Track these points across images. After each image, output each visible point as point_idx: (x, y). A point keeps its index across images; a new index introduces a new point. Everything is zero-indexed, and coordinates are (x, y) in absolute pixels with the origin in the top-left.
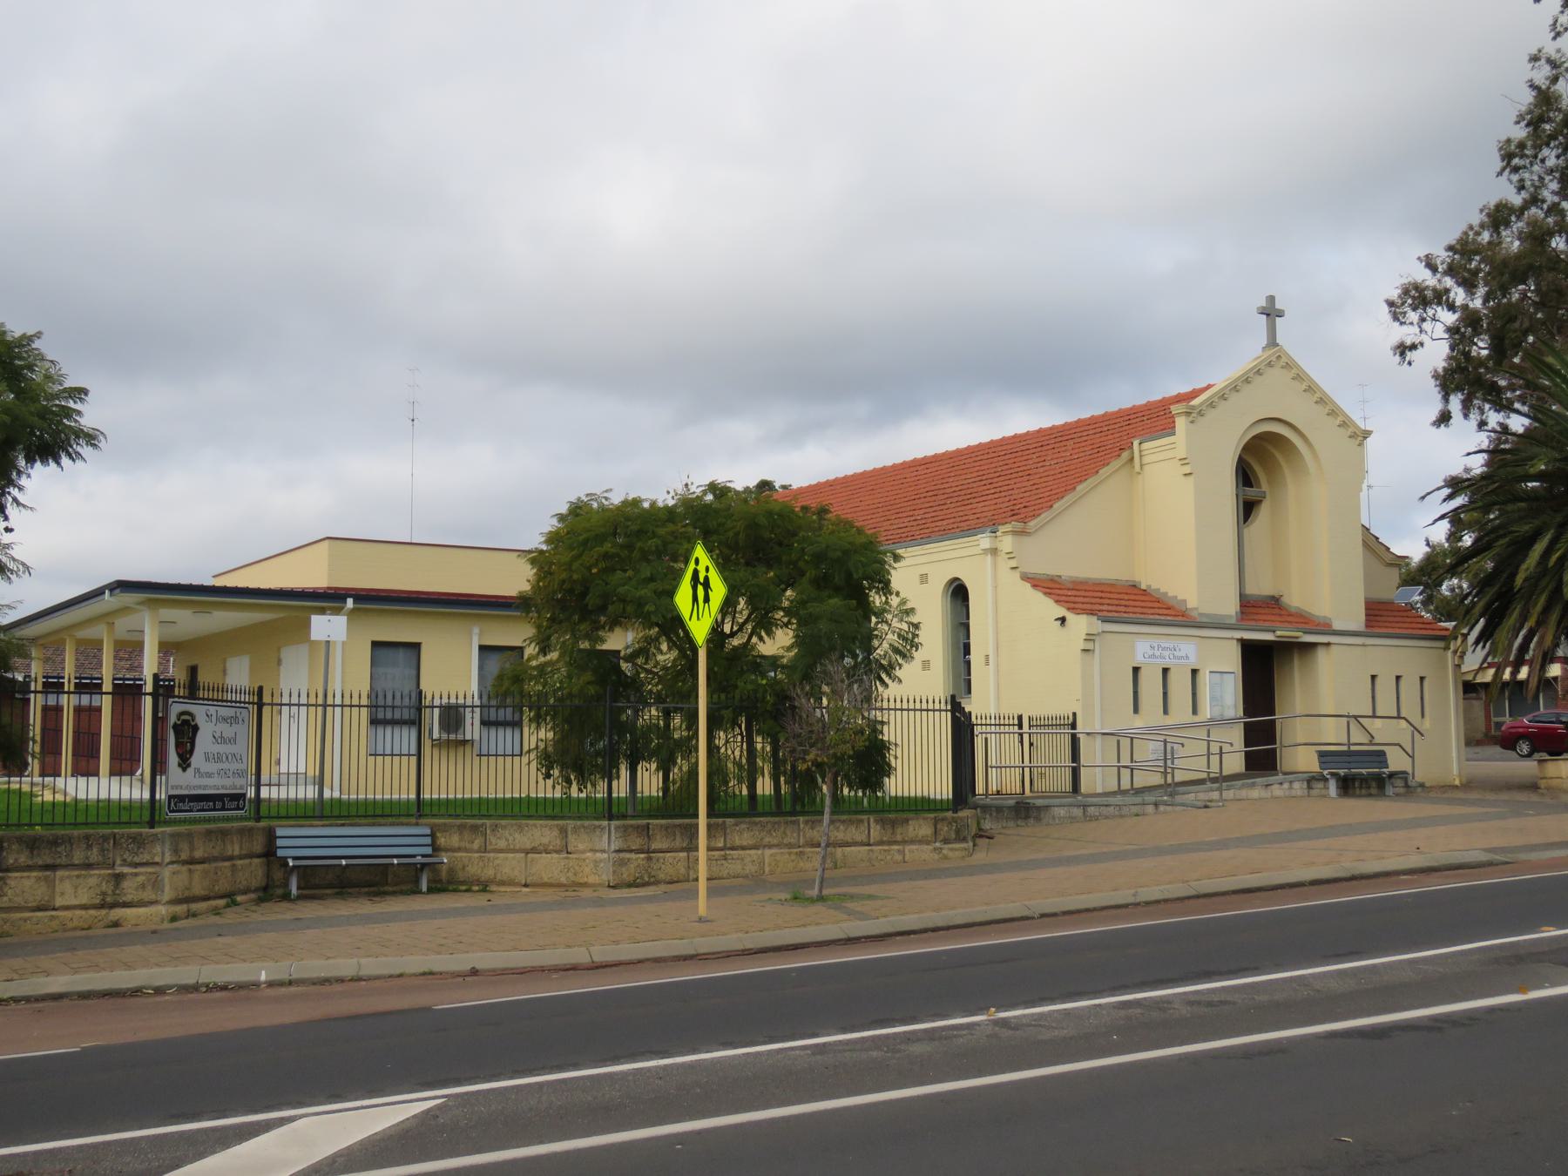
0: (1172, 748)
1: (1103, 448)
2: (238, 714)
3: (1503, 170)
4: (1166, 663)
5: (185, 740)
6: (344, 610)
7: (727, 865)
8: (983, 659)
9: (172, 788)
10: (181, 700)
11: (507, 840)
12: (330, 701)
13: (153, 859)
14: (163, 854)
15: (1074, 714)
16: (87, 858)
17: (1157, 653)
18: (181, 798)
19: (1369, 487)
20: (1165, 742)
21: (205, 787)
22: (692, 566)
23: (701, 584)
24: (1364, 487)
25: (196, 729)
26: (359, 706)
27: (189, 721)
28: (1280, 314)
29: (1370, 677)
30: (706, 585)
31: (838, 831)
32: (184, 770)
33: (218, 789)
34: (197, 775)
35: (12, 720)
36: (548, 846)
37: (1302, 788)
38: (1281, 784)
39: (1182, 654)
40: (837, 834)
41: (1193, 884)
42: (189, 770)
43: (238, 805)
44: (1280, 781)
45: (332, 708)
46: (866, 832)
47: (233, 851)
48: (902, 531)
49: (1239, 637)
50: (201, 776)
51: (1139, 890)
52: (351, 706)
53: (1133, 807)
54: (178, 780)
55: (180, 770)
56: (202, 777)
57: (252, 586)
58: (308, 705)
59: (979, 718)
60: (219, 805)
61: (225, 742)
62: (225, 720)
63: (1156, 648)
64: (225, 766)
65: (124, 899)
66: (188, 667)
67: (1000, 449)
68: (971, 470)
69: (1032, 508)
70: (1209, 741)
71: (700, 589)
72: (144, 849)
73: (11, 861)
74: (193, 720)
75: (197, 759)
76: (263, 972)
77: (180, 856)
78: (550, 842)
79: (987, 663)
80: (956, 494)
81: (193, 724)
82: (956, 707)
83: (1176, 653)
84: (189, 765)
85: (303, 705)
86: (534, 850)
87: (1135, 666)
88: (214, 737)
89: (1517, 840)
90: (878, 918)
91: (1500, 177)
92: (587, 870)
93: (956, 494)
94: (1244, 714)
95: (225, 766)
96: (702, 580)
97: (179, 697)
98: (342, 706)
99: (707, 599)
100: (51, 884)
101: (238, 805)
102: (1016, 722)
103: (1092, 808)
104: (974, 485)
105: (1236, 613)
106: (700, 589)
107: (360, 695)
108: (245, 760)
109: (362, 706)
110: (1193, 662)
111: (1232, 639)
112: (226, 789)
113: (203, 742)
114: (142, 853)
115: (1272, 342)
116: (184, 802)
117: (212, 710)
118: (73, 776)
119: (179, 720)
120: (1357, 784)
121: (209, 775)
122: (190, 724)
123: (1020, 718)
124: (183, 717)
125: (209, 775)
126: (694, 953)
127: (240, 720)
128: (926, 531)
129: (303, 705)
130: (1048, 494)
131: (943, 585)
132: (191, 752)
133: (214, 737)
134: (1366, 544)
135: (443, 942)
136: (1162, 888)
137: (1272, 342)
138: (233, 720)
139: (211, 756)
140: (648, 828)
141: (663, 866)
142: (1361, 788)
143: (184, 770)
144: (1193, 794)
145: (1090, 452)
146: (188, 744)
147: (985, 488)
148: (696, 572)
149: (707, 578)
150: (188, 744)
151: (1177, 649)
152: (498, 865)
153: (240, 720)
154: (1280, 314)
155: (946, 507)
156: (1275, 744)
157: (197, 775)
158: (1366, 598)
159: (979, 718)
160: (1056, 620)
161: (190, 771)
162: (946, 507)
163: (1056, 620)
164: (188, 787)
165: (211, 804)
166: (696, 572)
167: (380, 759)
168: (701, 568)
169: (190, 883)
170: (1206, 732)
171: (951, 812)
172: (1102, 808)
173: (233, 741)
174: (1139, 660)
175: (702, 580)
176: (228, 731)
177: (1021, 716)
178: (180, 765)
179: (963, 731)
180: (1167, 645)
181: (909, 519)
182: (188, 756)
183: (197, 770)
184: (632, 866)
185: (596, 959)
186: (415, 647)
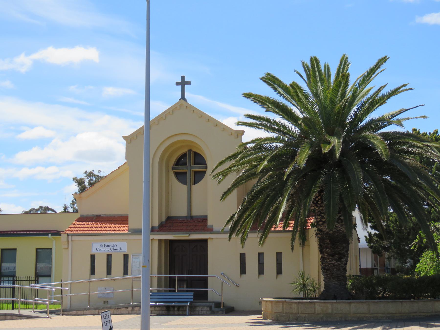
4: (109, 252)
17: (104, 248)
35: (204, 311)
38: (127, 308)
39: (118, 247)
44: (125, 307)
63: (104, 246)
83: (115, 248)
115: (183, 97)
120: (176, 309)
137: (183, 97)
142: (179, 311)
144: (74, 312)
151: (116, 246)
174: (93, 251)
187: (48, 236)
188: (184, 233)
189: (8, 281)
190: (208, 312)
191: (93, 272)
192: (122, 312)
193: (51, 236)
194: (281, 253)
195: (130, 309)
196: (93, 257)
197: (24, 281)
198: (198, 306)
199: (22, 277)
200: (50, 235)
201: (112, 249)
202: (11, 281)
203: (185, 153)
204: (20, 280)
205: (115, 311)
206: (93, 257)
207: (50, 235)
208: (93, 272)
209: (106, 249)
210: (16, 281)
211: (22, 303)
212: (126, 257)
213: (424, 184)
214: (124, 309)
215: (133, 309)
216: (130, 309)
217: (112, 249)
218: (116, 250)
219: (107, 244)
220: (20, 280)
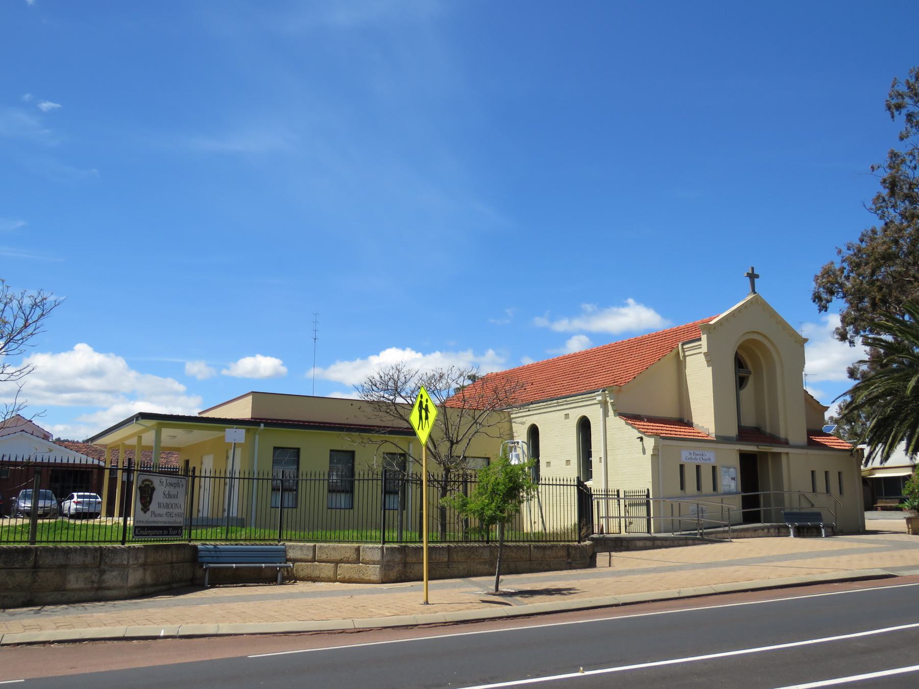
0: (702, 509)
1: (663, 348)
2: (180, 482)
3: (892, 114)
4: (698, 462)
5: (146, 495)
6: (259, 430)
7: (449, 570)
8: (598, 459)
9: (137, 522)
10: (157, 474)
11: (327, 554)
12: (203, 475)
13: (122, 562)
14: (128, 559)
15: (648, 490)
16: (85, 561)
17: (693, 457)
18: (143, 528)
19: (806, 375)
20: (698, 504)
21: (157, 522)
22: (419, 399)
23: (424, 409)
24: (804, 376)
25: (153, 489)
26: (210, 477)
27: (149, 485)
28: (757, 276)
29: (810, 472)
30: (427, 410)
31: (512, 552)
32: (145, 512)
33: (166, 523)
34: (153, 515)
36: (349, 558)
37: (774, 532)
38: (763, 530)
40: (512, 554)
41: (713, 586)
42: (148, 512)
43: (178, 532)
45: (243, 480)
46: (529, 553)
47: (172, 558)
48: (556, 391)
49: (738, 449)
50: (156, 516)
51: (682, 589)
52: (205, 477)
53: (680, 541)
54: (148, 519)
55: (142, 512)
56: (156, 516)
57: (229, 417)
58: (239, 478)
59: (595, 491)
60: (166, 532)
61: (171, 497)
62: (171, 485)
64: (171, 510)
65: (104, 585)
66: (185, 460)
67: (608, 349)
68: (594, 360)
69: (624, 379)
70: (722, 503)
71: (423, 412)
72: (118, 557)
73: (41, 562)
74: (152, 485)
75: (153, 506)
76: (163, 631)
77: (138, 561)
78: (350, 556)
79: (601, 462)
80: (585, 372)
81: (152, 486)
82: (581, 486)
84: (148, 510)
85: (237, 478)
86: (341, 561)
87: (681, 464)
88: (164, 494)
89: (900, 564)
90: (527, 604)
91: (906, 81)
92: (370, 572)
93: (585, 372)
94: (742, 491)
95: (171, 510)
96: (424, 407)
97: (181, 475)
98: (258, 479)
99: (427, 418)
100: (737, 535)
101: (178, 532)
102: (616, 493)
103: (658, 542)
104: (594, 368)
105: (736, 435)
106: (423, 412)
107: (216, 471)
108: (183, 507)
109: (260, 479)
110: (713, 462)
111: (734, 449)
112: (170, 523)
113: (158, 497)
114: (116, 559)
116: (144, 530)
117: (164, 479)
118: (244, 519)
119: (143, 484)
120: (805, 530)
121: (161, 515)
122: (150, 487)
123: (618, 491)
124: (145, 483)
125: (161, 515)
126: (416, 624)
127: (181, 485)
128: (569, 391)
129: (237, 478)
130: (633, 371)
131: (577, 421)
132: (150, 502)
133: (164, 494)
134: (806, 400)
135: (274, 614)
136: (695, 588)
138: (176, 485)
139: (162, 505)
140: (405, 549)
141: (413, 571)
143: (145, 512)
145: (656, 350)
146: (148, 498)
147: (600, 369)
148: (421, 403)
149: (427, 406)
150: (148, 498)
152: (322, 568)
153: (181, 485)
154: (757, 276)
155: (579, 379)
156: (758, 506)
157: (153, 515)
158: (807, 429)
159: (595, 491)
160: (638, 438)
161: (149, 513)
162: (579, 379)
163: (638, 438)
164: (147, 522)
165: (161, 531)
166: (421, 403)
167: (334, 511)
168: (424, 400)
169: (144, 577)
170: (720, 500)
171: (485, 543)
172: (663, 542)
173: (176, 496)
174: (683, 460)
175: (424, 407)
176: (173, 491)
177: (619, 490)
178: (142, 509)
179: (585, 499)
180: (698, 453)
181: (560, 385)
182: (148, 504)
183: (153, 513)
184: (395, 570)
185: (357, 626)
186: (297, 451)
187: (260, 426)
188: (768, 444)
189: (261, 479)
190: (830, 534)
191: (682, 487)
192: (760, 535)
193: (264, 426)
194: (828, 472)
195: (766, 531)
196: (682, 467)
197: (266, 481)
198: (27, 542)
199: (358, 474)
200: (262, 425)
201: (701, 459)
202: (574, 485)
203: (743, 386)
204: (207, 477)
205: (753, 534)
206: (682, 467)
207: (262, 425)
208: (682, 487)
209: (696, 459)
210: (576, 484)
211: (199, 511)
212: (714, 468)
213: (871, 407)
214: (760, 531)
215: (768, 532)
216: (766, 531)
217: (701, 459)
218: (705, 460)
219: (696, 453)
220: (559, 484)
